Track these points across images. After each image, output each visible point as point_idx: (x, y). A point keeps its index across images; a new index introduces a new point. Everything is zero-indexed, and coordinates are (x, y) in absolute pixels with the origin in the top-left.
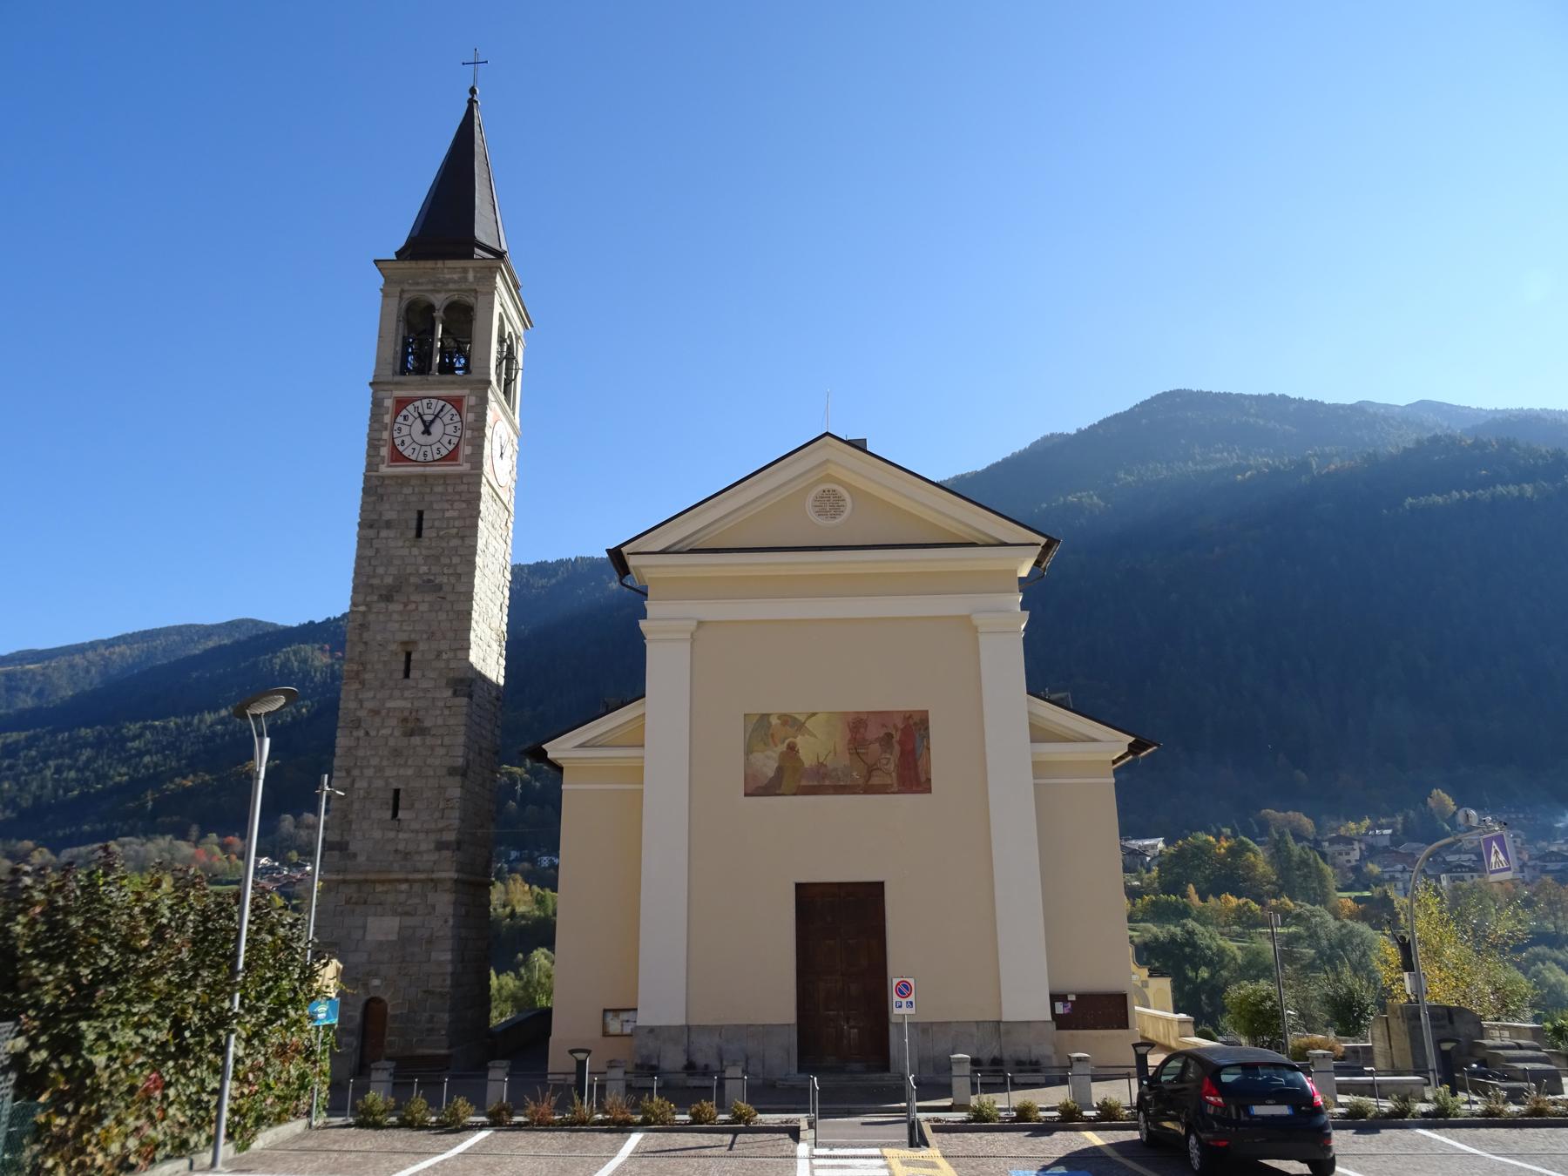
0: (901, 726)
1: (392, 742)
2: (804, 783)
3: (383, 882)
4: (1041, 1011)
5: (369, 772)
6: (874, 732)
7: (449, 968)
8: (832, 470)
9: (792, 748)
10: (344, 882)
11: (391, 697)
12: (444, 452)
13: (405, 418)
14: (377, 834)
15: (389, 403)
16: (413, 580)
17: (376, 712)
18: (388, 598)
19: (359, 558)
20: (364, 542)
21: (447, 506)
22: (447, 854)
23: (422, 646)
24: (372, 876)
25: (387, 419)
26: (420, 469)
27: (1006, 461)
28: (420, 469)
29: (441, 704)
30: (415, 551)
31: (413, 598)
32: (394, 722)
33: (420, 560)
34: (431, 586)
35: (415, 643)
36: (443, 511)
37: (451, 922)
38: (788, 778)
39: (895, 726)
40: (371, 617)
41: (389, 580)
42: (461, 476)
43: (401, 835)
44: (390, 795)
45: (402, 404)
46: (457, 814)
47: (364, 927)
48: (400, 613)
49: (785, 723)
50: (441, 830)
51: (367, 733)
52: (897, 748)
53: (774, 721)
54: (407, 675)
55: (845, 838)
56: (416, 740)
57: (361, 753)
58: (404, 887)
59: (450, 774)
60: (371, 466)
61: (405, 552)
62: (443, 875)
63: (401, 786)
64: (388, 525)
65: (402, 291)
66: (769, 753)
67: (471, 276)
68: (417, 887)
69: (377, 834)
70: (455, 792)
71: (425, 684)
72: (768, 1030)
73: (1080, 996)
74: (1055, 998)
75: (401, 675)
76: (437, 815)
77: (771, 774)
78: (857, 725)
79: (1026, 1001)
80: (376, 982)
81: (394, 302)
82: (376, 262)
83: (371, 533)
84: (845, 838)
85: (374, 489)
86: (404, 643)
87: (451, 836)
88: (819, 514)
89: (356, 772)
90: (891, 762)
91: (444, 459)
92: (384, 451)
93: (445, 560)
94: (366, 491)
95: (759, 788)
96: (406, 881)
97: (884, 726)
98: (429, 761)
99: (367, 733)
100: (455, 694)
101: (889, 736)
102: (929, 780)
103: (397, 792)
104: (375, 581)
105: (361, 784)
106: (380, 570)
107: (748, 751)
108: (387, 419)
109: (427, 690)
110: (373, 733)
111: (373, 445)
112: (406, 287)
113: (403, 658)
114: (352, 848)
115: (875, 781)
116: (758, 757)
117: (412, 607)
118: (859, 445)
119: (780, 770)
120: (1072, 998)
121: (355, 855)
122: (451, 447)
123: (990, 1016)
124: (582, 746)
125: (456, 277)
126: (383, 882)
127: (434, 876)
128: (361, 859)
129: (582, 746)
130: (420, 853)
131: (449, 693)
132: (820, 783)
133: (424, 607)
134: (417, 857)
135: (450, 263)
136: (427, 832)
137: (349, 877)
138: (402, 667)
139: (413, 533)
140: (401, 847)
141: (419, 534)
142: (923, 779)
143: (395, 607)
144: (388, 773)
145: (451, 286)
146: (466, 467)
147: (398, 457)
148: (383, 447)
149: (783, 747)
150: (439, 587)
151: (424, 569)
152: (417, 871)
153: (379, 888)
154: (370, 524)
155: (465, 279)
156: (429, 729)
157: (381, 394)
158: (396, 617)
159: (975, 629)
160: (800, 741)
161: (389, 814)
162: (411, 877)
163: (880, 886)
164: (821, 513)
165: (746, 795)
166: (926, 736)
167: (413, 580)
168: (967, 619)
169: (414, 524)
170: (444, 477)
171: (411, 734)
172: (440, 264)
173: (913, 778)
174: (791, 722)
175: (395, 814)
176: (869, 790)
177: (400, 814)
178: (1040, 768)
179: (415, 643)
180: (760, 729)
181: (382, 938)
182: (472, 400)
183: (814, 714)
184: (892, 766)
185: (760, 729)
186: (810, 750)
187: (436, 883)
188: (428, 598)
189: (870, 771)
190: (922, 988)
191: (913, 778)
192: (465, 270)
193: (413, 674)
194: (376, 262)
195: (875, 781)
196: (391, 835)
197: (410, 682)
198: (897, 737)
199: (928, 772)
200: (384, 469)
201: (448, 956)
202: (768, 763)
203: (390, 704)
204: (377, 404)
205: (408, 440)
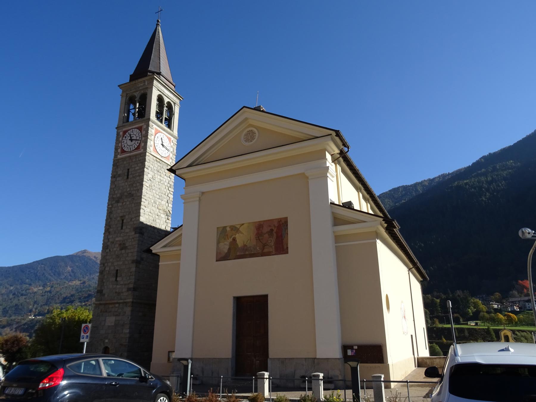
0: (276, 225)
1: (116, 253)
2: (238, 254)
3: (111, 304)
4: (337, 354)
5: (110, 264)
6: (266, 229)
7: (128, 335)
8: (251, 122)
9: (234, 239)
10: (101, 304)
11: (117, 237)
12: (136, 147)
13: (126, 137)
14: (111, 286)
15: (121, 133)
16: (125, 194)
17: (112, 243)
18: (118, 202)
19: (111, 188)
20: (112, 183)
21: (136, 166)
22: (130, 292)
23: (127, 217)
24: (108, 302)
25: (121, 139)
26: (128, 154)
27: (524, 139)
28: (128, 154)
29: (131, 237)
30: (126, 184)
31: (125, 200)
32: (117, 245)
33: (128, 186)
34: (131, 195)
35: (124, 216)
36: (135, 167)
37: (130, 318)
38: (231, 252)
39: (274, 226)
40: (113, 209)
41: (118, 195)
42: (140, 154)
43: (118, 286)
44: (115, 272)
45: (125, 132)
46: (133, 277)
47: (105, 321)
48: (121, 206)
49: (232, 229)
50: (129, 284)
51: (110, 250)
52: (275, 234)
53: (228, 229)
54: (122, 229)
55: (252, 276)
56: (123, 251)
57: (108, 257)
58: (117, 305)
59: (132, 263)
60: (115, 156)
61: (123, 184)
62: (128, 300)
63: (119, 269)
64: (119, 176)
65: (127, 94)
66: (226, 242)
67: (146, 83)
68: (121, 304)
69: (111, 286)
70: (133, 269)
71: (127, 231)
72: (220, 360)
73: (359, 346)
74: (345, 348)
75: (120, 228)
76: (128, 278)
77: (226, 251)
78: (259, 226)
79: (329, 348)
80: (107, 341)
81: (124, 98)
82: (119, 86)
83: (114, 179)
84: (252, 276)
85: (116, 164)
86: (122, 217)
87: (131, 286)
88: (246, 141)
89: (106, 265)
90: (272, 242)
91: (136, 149)
92: (119, 150)
93: (134, 185)
94: (114, 165)
95: (222, 257)
96: (117, 303)
97: (270, 226)
98: (127, 258)
99: (110, 250)
100: (135, 234)
101: (272, 230)
102: (287, 248)
103: (117, 270)
104: (115, 196)
105: (107, 269)
106: (116, 192)
107: (218, 243)
108: (121, 139)
109: (127, 233)
110: (111, 250)
111: (116, 149)
112: (128, 92)
113: (121, 222)
114: (104, 292)
115: (266, 250)
116: (221, 244)
117: (124, 204)
118: (258, 109)
119: (229, 249)
120: (356, 347)
121: (104, 295)
122: (138, 145)
123: (311, 356)
124: (165, 246)
125: (142, 85)
126: (111, 304)
127: (125, 301)
128: (106, 296)
129: (165, 246)
130: (122, 293)
131: (134, 233)
132: (245, 253)
133: (128, 203)
134: (122, 294)
135: (140, 80)
136: (125, 285)
137: (101, 302)
138: (120, 225)
139: (126, 177)
140: (117, 291)
141: (128, 178)
142: (285, 247)
143: (120, 204)
144: (116, 264)
145: (141, 88)
146: (142, 151)
147: (123, 151)
148: (119, 149)
149: (231, 240)
150: (133, 195)
151: (129, 189)
152: (121, 299)
153: (111, 306)
154: (114, 176)
155: (145, 84)
156: (127, 247)
157: (119, 131)
158: (120, 208)
159: (307, 178)
160: (237, 236)
161: (114, 279)
162: (119, 301)
163: (265, 297)
164: (247, 140)
165: (217, 261)
166: (287, 229)
167: (125, 194)
168: (303, 174)
169: (126, 174)
170: (136, 155)
171: (121, 249)
172: (137, 81)
173: (281, 248)
174: (235, 229)
175: (116, 279)
176: (263, 254)
177: (118, 279)
178: (337, 238)
179: (124, 216)
180: (223, 233)
181: (110, 324)
182: (145, 127)
183: (243, 224)
184: (272, 244)
185: (223, 233)
186: (241, 239)
187: (126, 303)
188: (129, 200)
189: (264, 246)
190: (282, 341)
191: (281, 248)
192: (144, 81)
193: (124, 227)
194: (119, 86)
195: (266, 250)
196: (115, 286)
197: (123, 231)
198: (275, 230)
199: (287, 244)
200: (119, 157)
201: (128, 331)
202: (225, 247)
203: (117, 239)
204: (118, 134)
205: (126, 145)
